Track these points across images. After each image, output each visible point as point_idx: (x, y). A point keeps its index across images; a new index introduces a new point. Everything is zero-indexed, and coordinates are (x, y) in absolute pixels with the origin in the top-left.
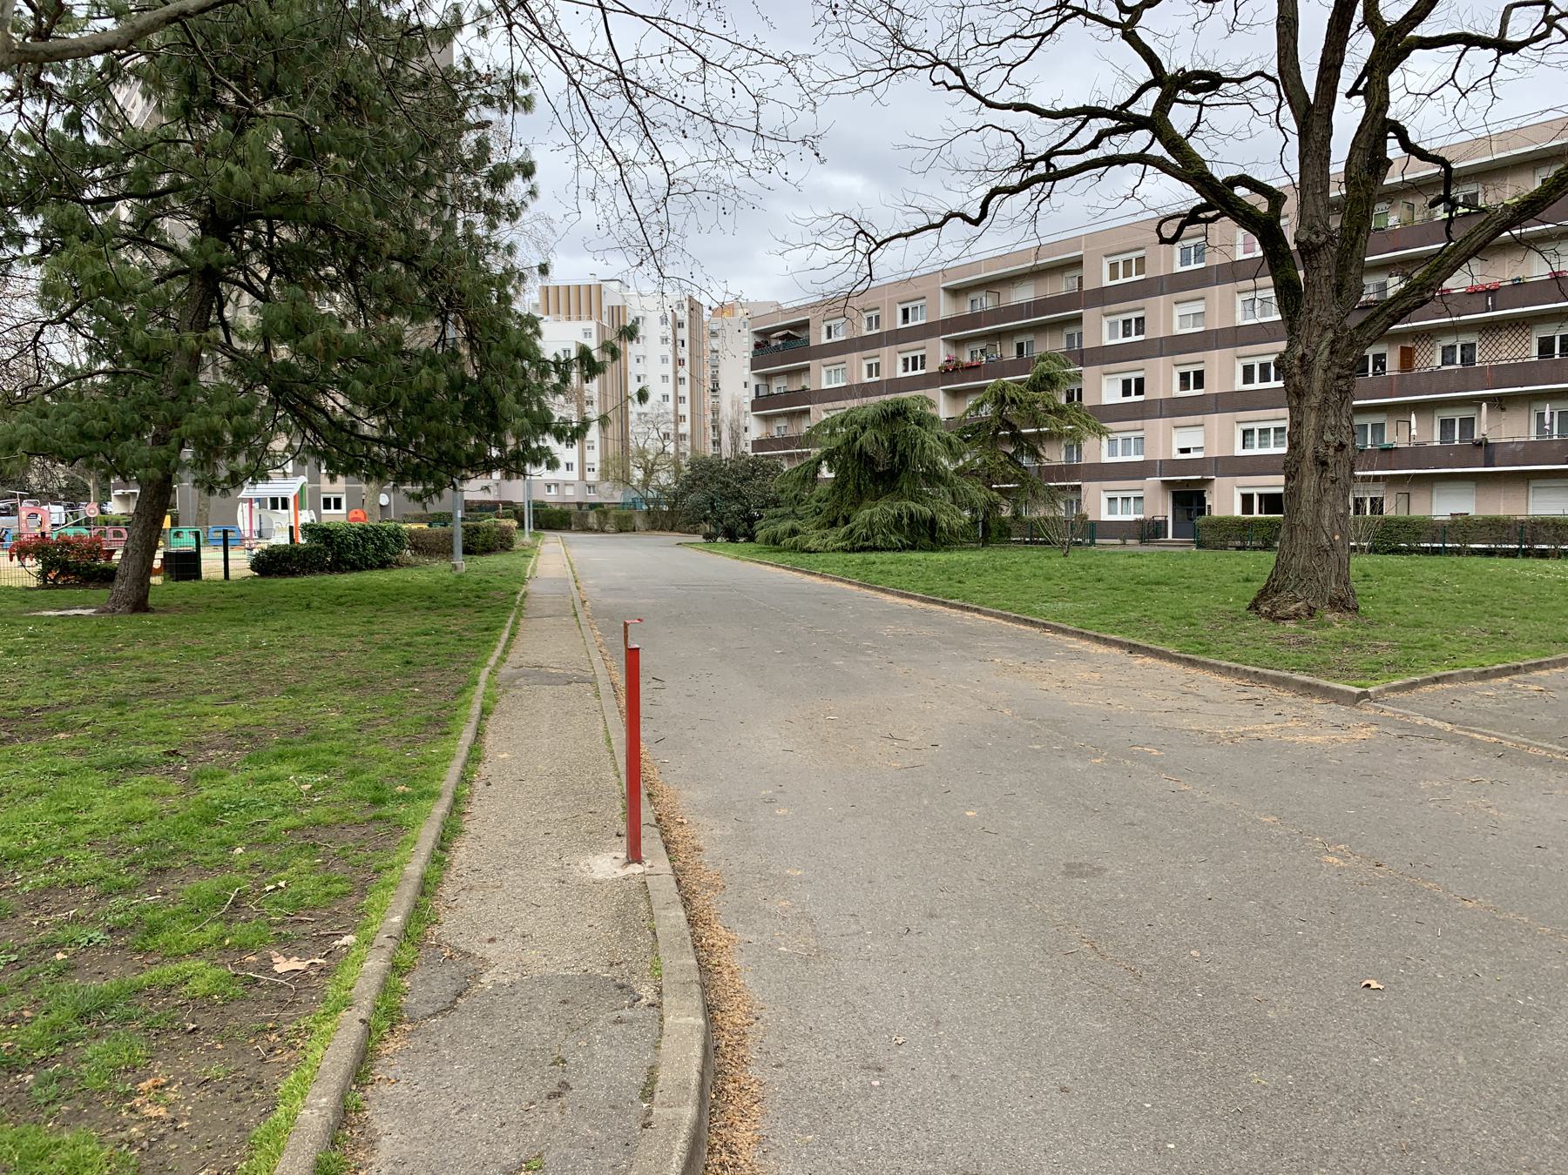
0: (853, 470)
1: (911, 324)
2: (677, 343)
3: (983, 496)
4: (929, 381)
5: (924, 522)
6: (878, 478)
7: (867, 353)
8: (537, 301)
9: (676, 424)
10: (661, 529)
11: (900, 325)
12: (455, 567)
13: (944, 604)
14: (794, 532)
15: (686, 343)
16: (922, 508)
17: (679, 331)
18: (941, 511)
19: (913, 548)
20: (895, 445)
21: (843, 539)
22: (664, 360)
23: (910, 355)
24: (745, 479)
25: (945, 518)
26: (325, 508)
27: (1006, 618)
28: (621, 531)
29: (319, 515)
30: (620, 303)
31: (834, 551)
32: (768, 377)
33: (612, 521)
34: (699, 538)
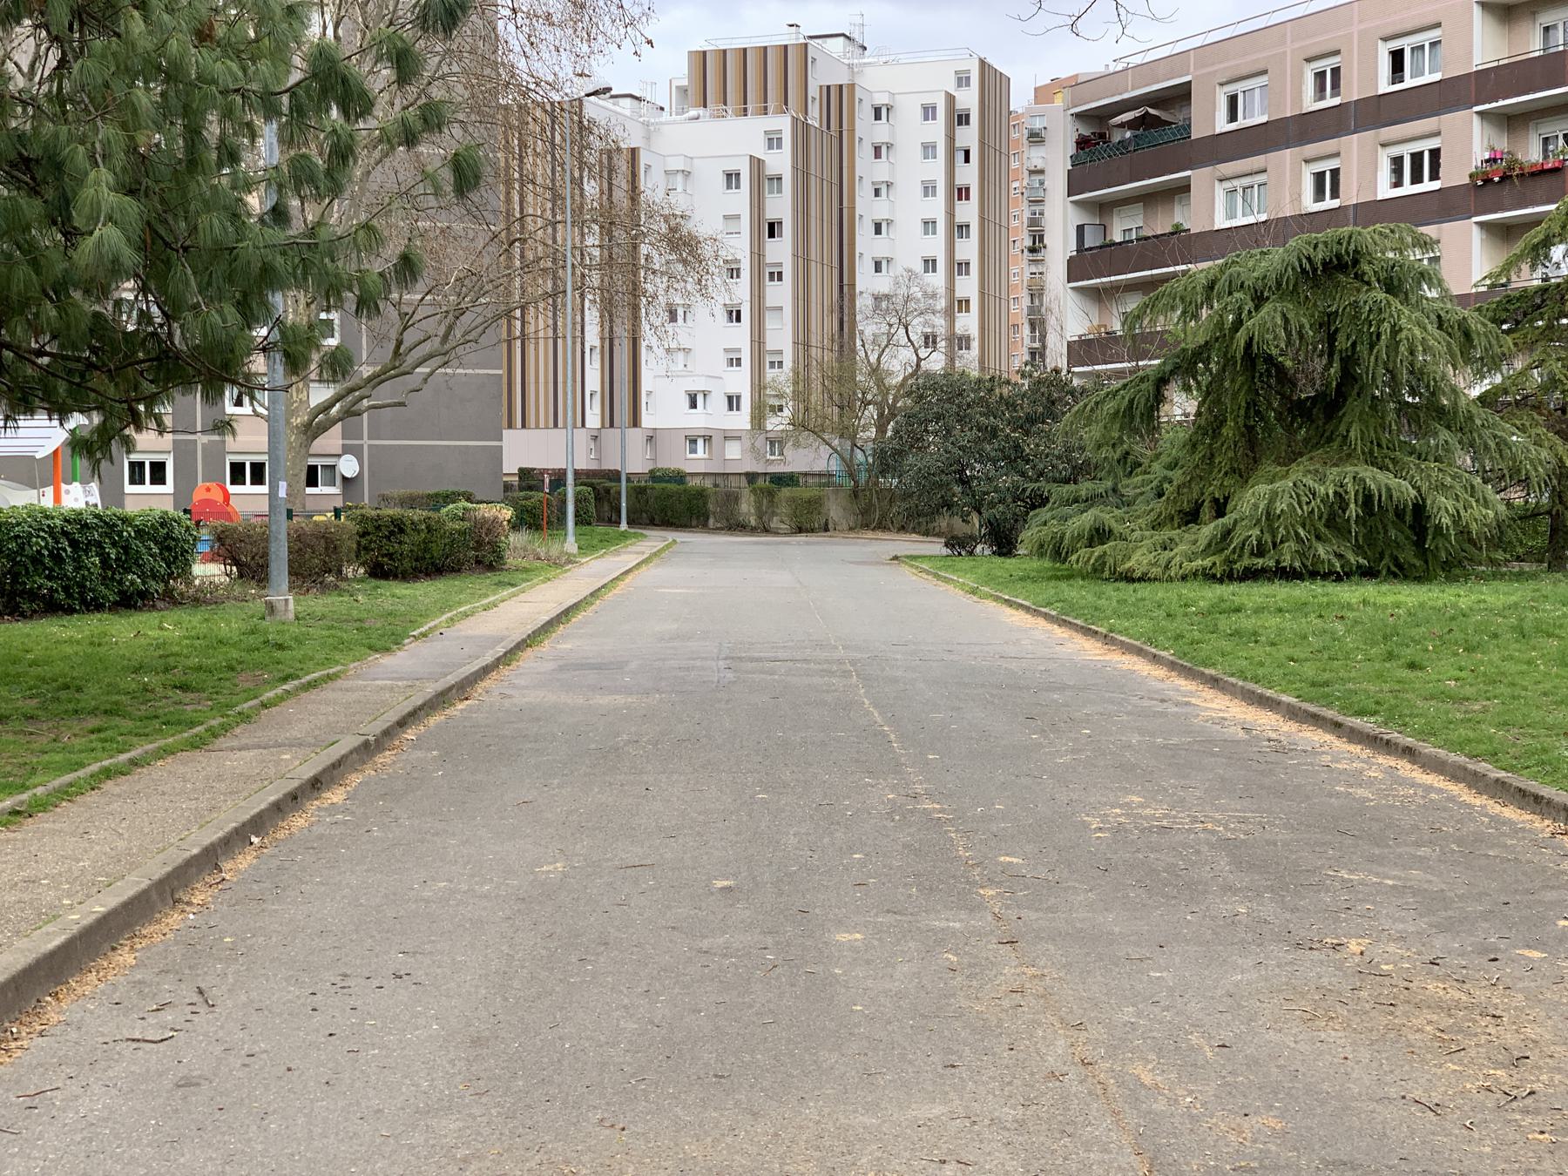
0: (1235, 396)
1: (1409, 82)
2: (956, 154)
3: (1544, 454)
4: (1447, 206)
5: (1399, 514)
6: (1300, 410)
7: (1311, 149)
8: (685, 82)
9: (950, 314)
10: (882, 526)
11: (1385, 86)
12: (271, 608)
13: (1336, 727)
14: (1100, 535)
15: (974, 156)
16: (1393, 482)
17: (961, 131)
18: (1442, 487)
19: (1369, 573)
20: (1332, 338)
21: (1206, 552)
22: (929, 189)
23: (1406, 151)
24: (1031, 420)
25: (1450, 504)
26: (132, 482)
27: (1475, 781)
28: (800, 530)
29: (112, 494)
30: (844, 81)
31: (1184, 578)
32: (1104, 208)
33: (784, 509)
34: (937, 547)
